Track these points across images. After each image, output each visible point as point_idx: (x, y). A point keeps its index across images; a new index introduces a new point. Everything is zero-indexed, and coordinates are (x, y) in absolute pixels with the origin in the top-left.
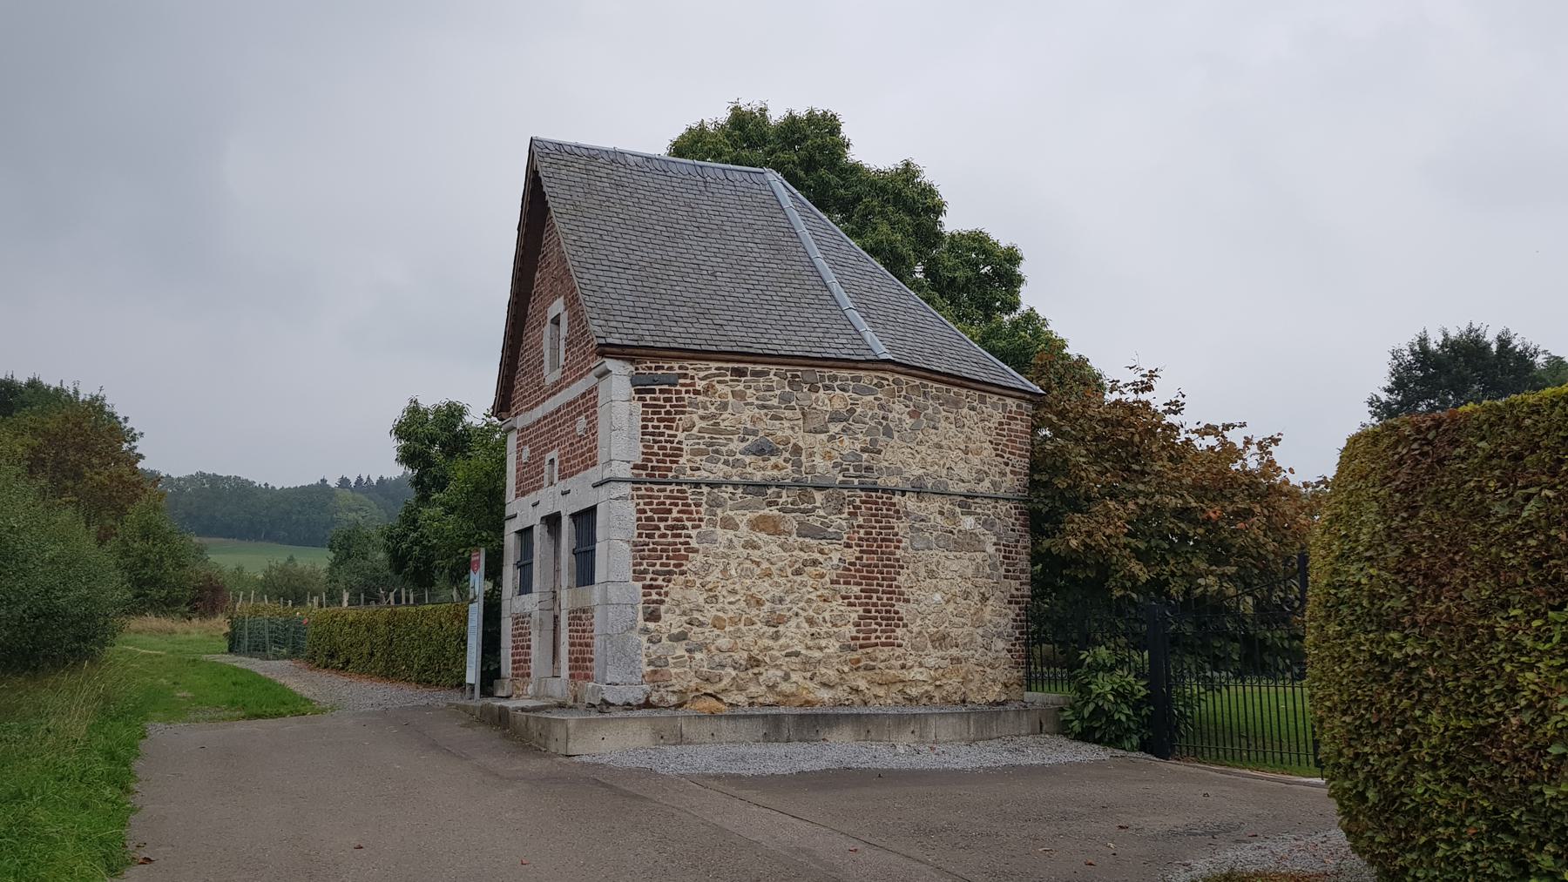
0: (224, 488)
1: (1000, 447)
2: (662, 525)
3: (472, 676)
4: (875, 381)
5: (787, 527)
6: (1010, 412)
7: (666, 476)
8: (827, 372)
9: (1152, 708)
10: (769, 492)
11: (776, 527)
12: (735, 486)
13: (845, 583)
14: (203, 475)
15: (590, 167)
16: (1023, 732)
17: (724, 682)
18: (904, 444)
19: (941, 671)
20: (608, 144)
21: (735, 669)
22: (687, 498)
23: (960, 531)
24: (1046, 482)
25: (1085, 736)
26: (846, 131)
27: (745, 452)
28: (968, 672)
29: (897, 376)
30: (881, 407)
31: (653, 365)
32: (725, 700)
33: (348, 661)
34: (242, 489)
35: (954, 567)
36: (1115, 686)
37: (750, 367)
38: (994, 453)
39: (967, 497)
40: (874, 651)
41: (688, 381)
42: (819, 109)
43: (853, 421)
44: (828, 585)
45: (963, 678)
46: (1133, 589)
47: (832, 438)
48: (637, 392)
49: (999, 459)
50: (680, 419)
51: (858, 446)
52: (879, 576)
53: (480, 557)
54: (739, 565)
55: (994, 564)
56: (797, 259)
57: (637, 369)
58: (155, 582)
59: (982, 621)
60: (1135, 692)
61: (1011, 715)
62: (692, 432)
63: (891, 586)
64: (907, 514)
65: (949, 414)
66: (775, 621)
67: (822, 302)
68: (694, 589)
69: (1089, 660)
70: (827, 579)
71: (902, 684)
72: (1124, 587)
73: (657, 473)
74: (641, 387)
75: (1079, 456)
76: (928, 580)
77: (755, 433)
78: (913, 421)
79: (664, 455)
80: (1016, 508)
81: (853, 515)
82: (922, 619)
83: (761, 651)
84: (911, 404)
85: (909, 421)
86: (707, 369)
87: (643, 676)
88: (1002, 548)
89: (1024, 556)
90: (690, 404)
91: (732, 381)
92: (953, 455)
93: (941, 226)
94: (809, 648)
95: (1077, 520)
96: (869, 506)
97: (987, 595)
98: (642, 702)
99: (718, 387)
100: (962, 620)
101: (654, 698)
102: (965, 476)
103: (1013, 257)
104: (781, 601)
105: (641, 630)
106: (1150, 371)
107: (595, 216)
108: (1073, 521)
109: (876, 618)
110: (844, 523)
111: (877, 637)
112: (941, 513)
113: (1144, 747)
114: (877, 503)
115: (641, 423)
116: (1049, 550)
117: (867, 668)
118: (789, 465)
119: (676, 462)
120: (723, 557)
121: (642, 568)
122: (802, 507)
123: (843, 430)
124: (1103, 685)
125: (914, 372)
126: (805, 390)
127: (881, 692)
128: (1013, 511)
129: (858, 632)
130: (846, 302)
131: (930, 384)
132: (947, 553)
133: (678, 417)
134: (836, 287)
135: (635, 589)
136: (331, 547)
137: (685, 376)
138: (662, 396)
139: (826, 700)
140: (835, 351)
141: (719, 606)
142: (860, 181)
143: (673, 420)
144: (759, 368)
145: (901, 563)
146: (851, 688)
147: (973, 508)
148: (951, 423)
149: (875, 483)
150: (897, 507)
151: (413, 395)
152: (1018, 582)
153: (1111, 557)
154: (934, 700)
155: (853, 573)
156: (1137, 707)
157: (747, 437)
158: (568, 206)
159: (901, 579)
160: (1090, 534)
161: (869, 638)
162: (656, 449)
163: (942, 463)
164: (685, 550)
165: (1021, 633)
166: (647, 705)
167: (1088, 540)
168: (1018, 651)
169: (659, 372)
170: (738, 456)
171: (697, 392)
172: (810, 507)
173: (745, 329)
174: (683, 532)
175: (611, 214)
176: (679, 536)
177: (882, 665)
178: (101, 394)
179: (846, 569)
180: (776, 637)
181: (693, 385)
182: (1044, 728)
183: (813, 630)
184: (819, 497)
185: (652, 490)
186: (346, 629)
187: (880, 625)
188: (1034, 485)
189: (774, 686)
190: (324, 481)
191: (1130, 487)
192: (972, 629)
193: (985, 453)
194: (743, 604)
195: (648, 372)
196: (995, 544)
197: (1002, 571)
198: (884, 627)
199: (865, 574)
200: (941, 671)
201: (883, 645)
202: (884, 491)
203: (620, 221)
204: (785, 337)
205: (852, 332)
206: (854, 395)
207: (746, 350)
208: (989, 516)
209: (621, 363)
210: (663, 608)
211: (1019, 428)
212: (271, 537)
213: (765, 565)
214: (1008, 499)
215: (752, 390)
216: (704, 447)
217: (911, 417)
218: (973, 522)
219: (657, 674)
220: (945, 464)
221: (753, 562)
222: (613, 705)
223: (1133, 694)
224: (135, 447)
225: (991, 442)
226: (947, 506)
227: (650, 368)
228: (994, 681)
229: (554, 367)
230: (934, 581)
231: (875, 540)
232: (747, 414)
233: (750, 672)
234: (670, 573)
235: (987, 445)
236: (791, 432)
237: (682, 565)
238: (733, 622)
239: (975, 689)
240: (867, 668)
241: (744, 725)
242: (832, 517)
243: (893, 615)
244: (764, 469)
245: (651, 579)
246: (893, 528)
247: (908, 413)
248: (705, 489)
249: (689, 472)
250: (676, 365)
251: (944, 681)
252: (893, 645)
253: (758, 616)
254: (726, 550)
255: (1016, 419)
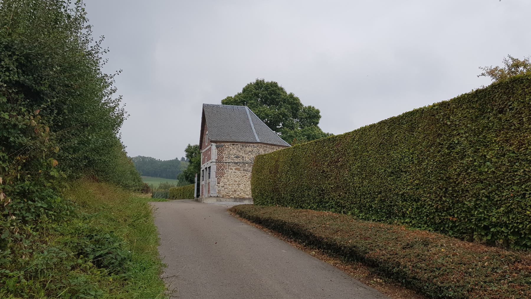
0: (146, 161)
3: (195, 196)
8: (248, 144)
11: (239, 169)
14: (140, 157)
30: (258, 150)
33: (176, 198)
34: (152, 161)
47: (249, 155)
51: (254, 156)
53: (196, 175)
66: (239, 185)
74: (217, 147)
77: (236, 154)
101: (219, 196)
104: (240, 181)
134: (253, 128)
136: (178, 179)
144: (237, 144)
151: (189, 143)
166: (217, 197)
180: (239, 187)
184: (247, 165)
186: (176, 191)
189: (239, 195)
190: (177, 158)
194: (233, 182)
212: (161, 176)
213: (237, 176)
219: (219, 192)
224: (125, 150)
229: (207, 142)
238: (232, 184)
248: (227, 163)
250: (223, 143)
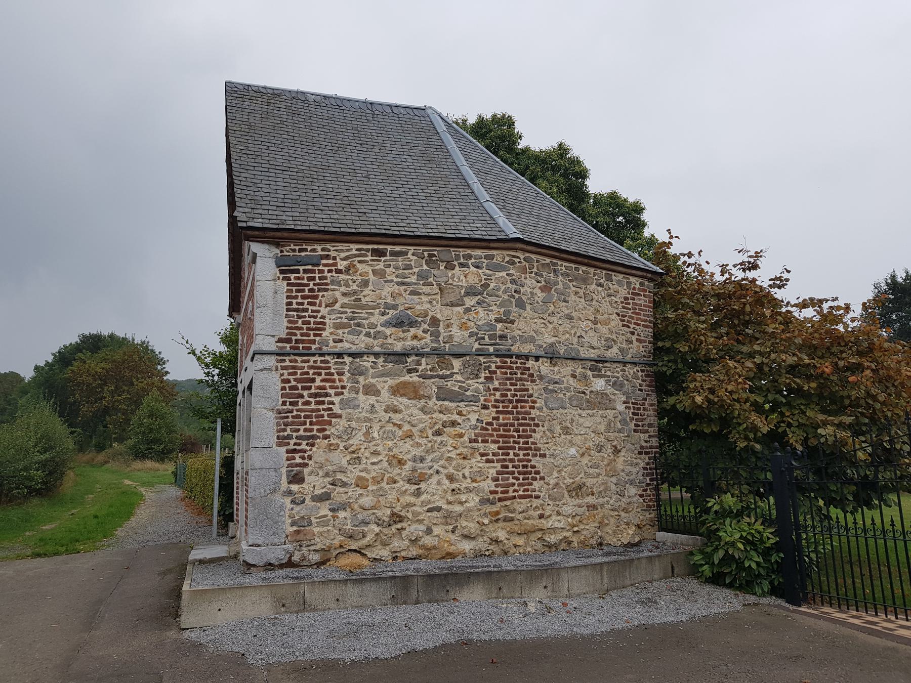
1: (626, 319)
2: (305, 393)
4: (507, 259)
5: (427, 392)
6: (634, 289)
7: (310, 348)
8: (463, 252)
9: (782, 555)
10: (409, 360)
11: (416, 391)
12: (377, 355)
13: (483, 441)
15: (272, 101)
16: (656, 577)
17: (368, 539)
18: (537, 315)
19: (578, 518)
20: (293, 87)
21: (378, 525)
22: (329, 368)
23: (591, 392)
24: (669, 348)
25: (716, 580)
26: (518, 128)
27: (387, 324)
28: (604, 517)
29: (528, 255)
30: (514, 282)
31: (297, 248)
32: (369, 555)
35: (588, 424)
36: (744, 534)
37: (389, 248)
38: (621, 325)
39: (597, 361)
40: (513, 503)
41: (331, 262)
42: (500, 112)
43: (487, 294)
44: (467, 444)
45: (600, 523)
46: (756, 440)
47: (468, 310)
48: (282, 272)
49: (625, 328)
50: (323, 296)
51: (492, 317)
52: (515, 434)
54: (381, 427)
55: (624, 419)
56: (446, 167)
57: (282, 251)
58: (156, 441)
59: (615, 471)
60: (765, 539)
61: (644, 561)
62: (335, 308)
63: (527, 443)
64: (541, 378)
65: (578, 290)
66: (416, 479)
67: (463, 197)
68: (338, 452)
69: (716, 507)
70: (466, 438)
71: (541, 533)
72: (746, 438)
73: (301, 346)
74: (286, 268)
75: (696, 324)
76: (563, 436)
77: (395, 307)
78: (544, 294)
79: (308, 329)
80: (642, 371)
81: (489, 379)
82: (559, 472)
83: (403, 508)
84: (542, 280)
85: (540, 295)
86: (348, 250)
87: (287, 536)
88: (631, 406)
89: (652, 412)
90: (333, 282)
91: (373, 260)
92: (583, 325)
93: (586, 188)
94: (450, 503)
95: (698, 379)
96: (503, 370)
97: (619, 448)
98: (284, 562)
99: (359, 266)
100: (597, 470)
101: (296, 558)
102: (595, 343)
103: (638, 209)
104: (422, 460)
105: (285, 492)
106: (756, 253)
107: (266, 133)
108: (695, 380)
109: (513, 473)
110: (481, 387)
111: (515, 491)
112: (574, 376)
113: (775, 591)
114: (511, 368)
115: (286, 301)
116: (674, 406)
117: (506, 520)
118: (428, 336)
119: (320, 335)
120: (365, 421)
121: (286, 434)
122: (441, 373)
123: (478, 303)
124: (731, 532)
125: (543, 251)
126: (441, 268)
127: (520, 541)
128: (640, 374)
129: (496, 486)
130: (483, 194)
131: (560, 263)
132: (580, 411)
133: (321, 294)
135: (278, 454)
137: (327, 257)
138: (306, 276)
139: (467, 551)
140: (469, 232)
141: (362, 467)
142: (528, 157)
143: (316, 297)
144: (398, 248)
145: (536, 421)
146: (491, 539)
147: (603, 373)
148: (581, 297)
149: (509, 350)
150: (531, 371)
152: (647, 435)
153: (732, 412)
154: (572, 545)
155: (490, 432)
156: (766, 553)
157: (387, 311)
158: (242, 126)
159: (537, 436)
160: (712, 391)
161: (507, 492)
162: (300, 324)
163: (573, 332)
164: (329, 415)
165: (651, 480)
166: (290, 564)
167: (711, 397)
168: (650, 496)
169: (303, 254)
170: (379, 328)
171: (339, 271)
172: (448, 373)
173: (387, 216)
174: (327, 399)
175: (282, 132)
176: (323, 403)
177: (519, 516)
178: (147, 340)
179: (483, 429)
180: (418, 493)
181: (335, 265)
182: (675, 572)
183: (454, 486)
184: (457, 364)
185: (296, 361)
187: (518, 479)
188: (658, 352)
191: (745, 349)
192: (606, 478)
193: (613, 324)
194: (385, 464)
195: (291, 254)
196: (624, 402)
197: (632, 426)
198: (521, 481)
199: (502, 432)
200: (578, 518)
201: (521, 497)
202: (518, 356)
203: (289, 137)
204: (424, 223)
205: (489, 219)
206: (487, 272)
207: (383, 231)
208: (618, 378)
209: (266, 246)
210: (306, 471)
211: (642, 302)
214: (635, 364)
215: (392, 269)
216: (346, 321)
217: (542, 291)
218: (604, 383)
220: (575, 333)
221: (395, 424)
222: (254, 566)
223: (762, 541)
224: (164, 368)
225: (618, 314)
226: (579, 370)
227: (294, 251)
228: (627, 524)
230: (569, 437)
231: (510, 401)
232: (387, 290)
233: (393, 528)
234: (314, 437)
235: (614, 316)
236: (429, 306)
237: (324, 430)
238: (376, 481)
239: (611, 532)
240: (506, 520)
241: (371, 590)
242: (470, 382)
243: (529, 469)
244: (404, 339)
245: (295, 444)
246: (527, 390)
247: (540, 288)
248: (347, 360)
249: (331, 344)
250: (319, 247)
251: (582, 527)
252: (531, 496)
253: (400, 474)
254: (368, 415)
255: (639, 295)
